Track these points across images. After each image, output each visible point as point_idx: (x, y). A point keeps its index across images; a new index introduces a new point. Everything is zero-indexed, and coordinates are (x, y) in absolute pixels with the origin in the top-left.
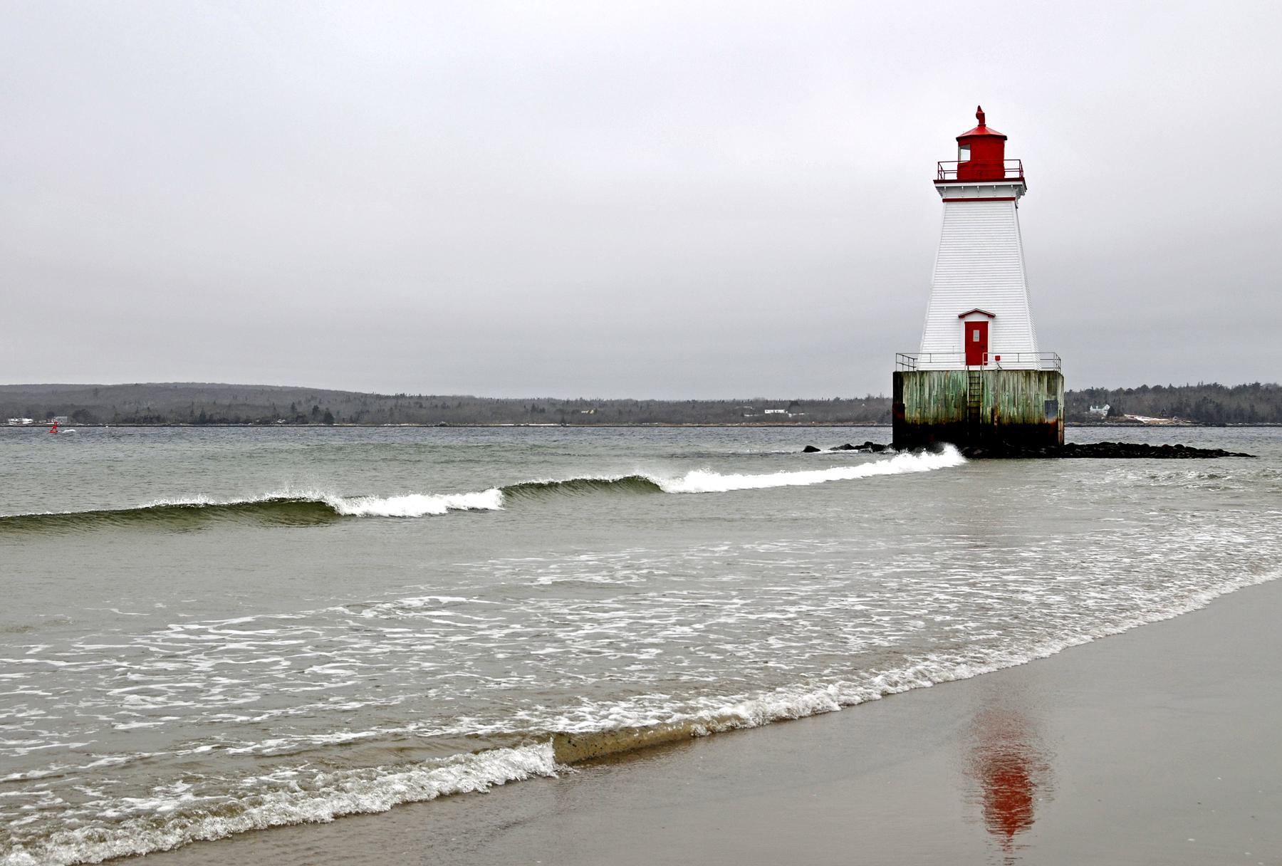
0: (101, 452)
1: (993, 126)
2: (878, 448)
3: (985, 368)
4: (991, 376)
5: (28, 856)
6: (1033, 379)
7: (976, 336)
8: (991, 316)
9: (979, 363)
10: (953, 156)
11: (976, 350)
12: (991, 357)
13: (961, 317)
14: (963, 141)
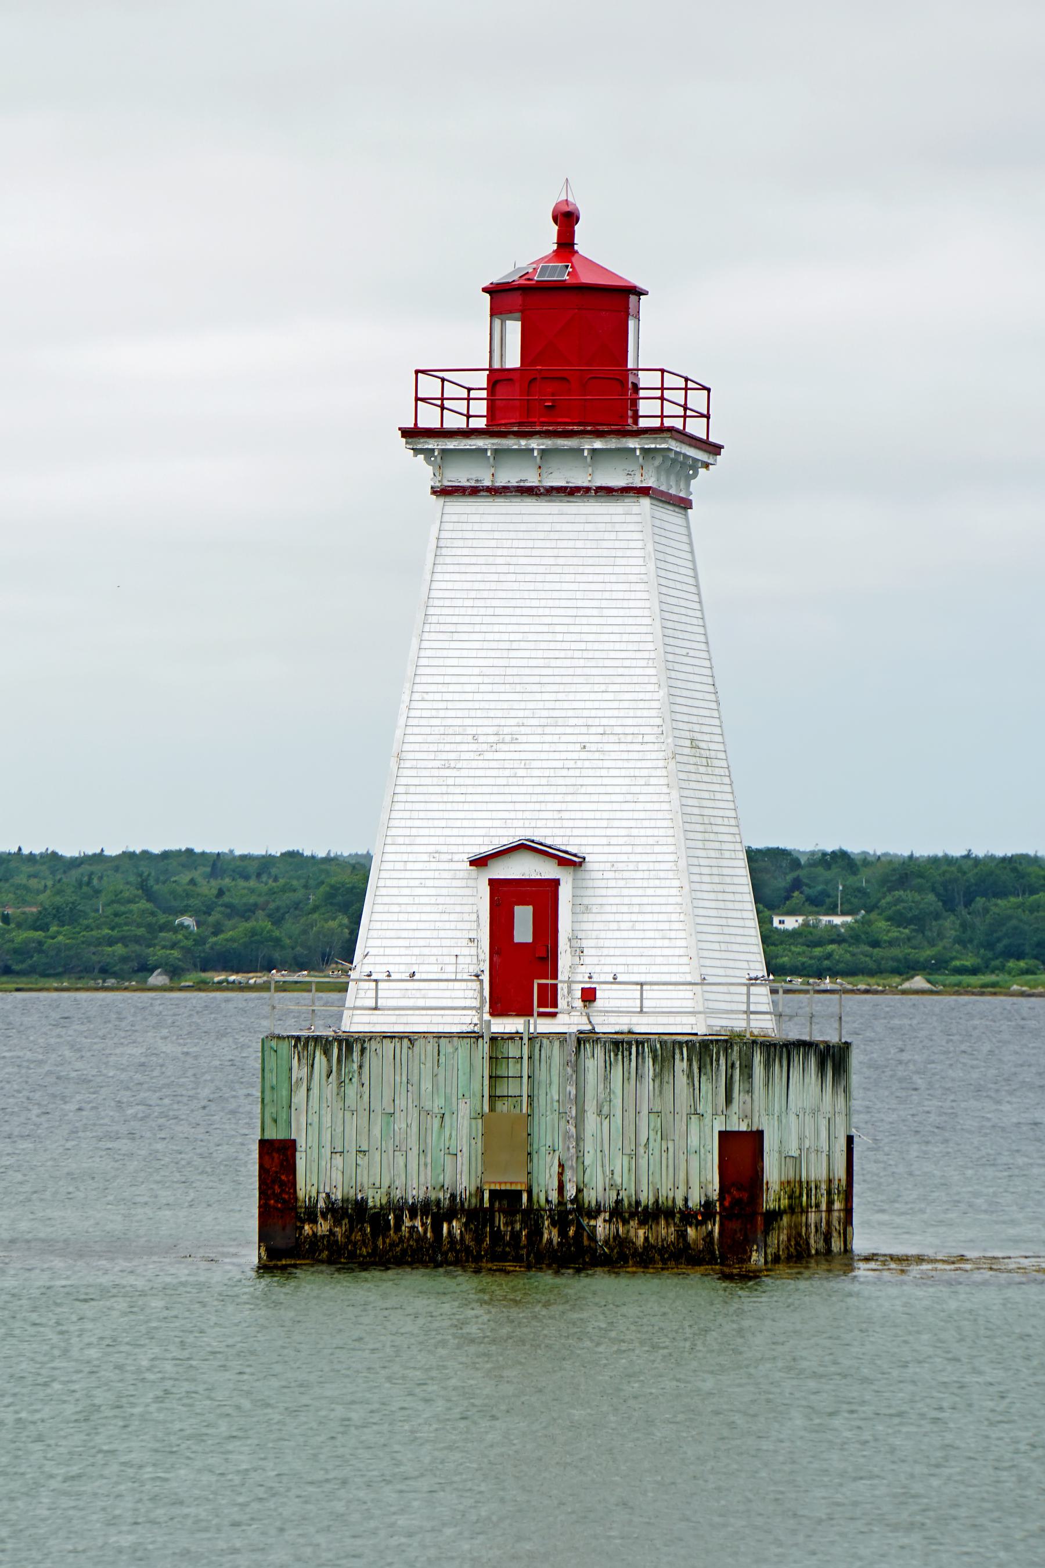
0: (980, 1276)
1: (602, 250)
3: (544, 1026)
4: (556, 1053)
7: (523, 931)
8: (570, 862)
9: (525, 1011)
10: (478, 345)
11: (522, 967)
12: (568, 997)
13: (480, 862)
14: (503, 297)
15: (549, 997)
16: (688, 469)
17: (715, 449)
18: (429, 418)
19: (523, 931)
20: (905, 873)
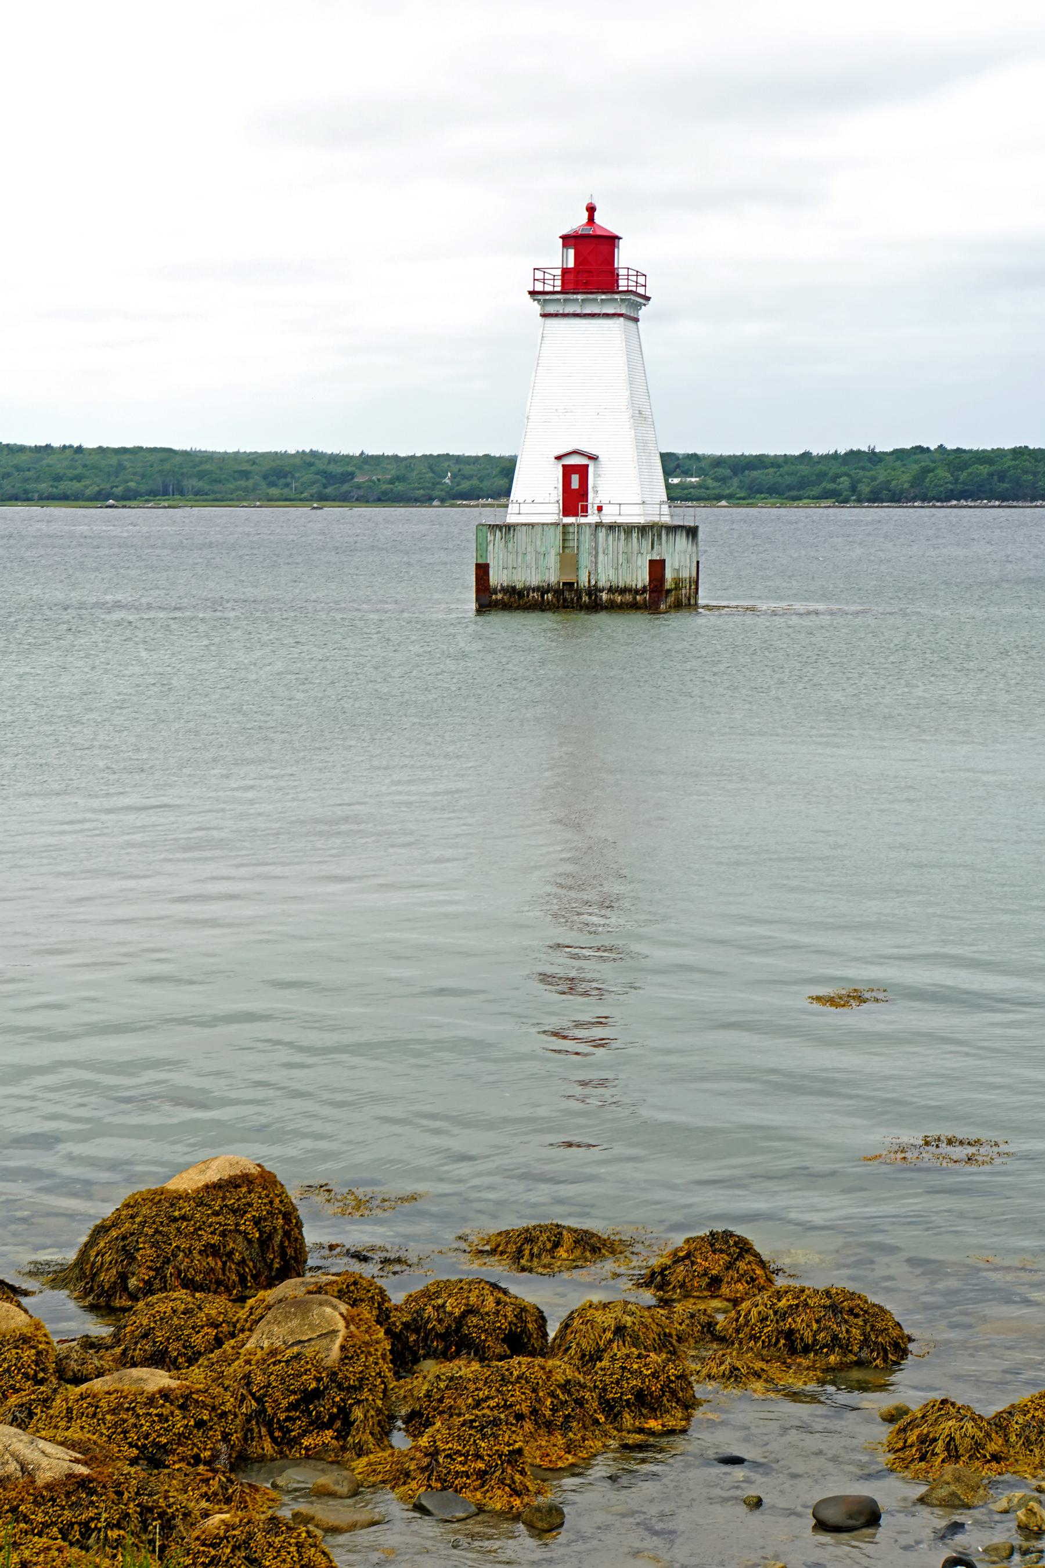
1: (605, 221)
2: (333, 1495)
3: (583, 520)
4: (587, 531)
5: (899, 1484)
6: (635, 535)
7: (575, 484)
8: (593, 458)
10: (558, 259)
11: (574, 498)
12: (592, 509)
13: (559, 458)
14: (568, 240)
15: (585, 509)
16: (637, 306)
17: (648, 299)
18: (539, 287)
19: (575, 484)
20: (719, 462)
